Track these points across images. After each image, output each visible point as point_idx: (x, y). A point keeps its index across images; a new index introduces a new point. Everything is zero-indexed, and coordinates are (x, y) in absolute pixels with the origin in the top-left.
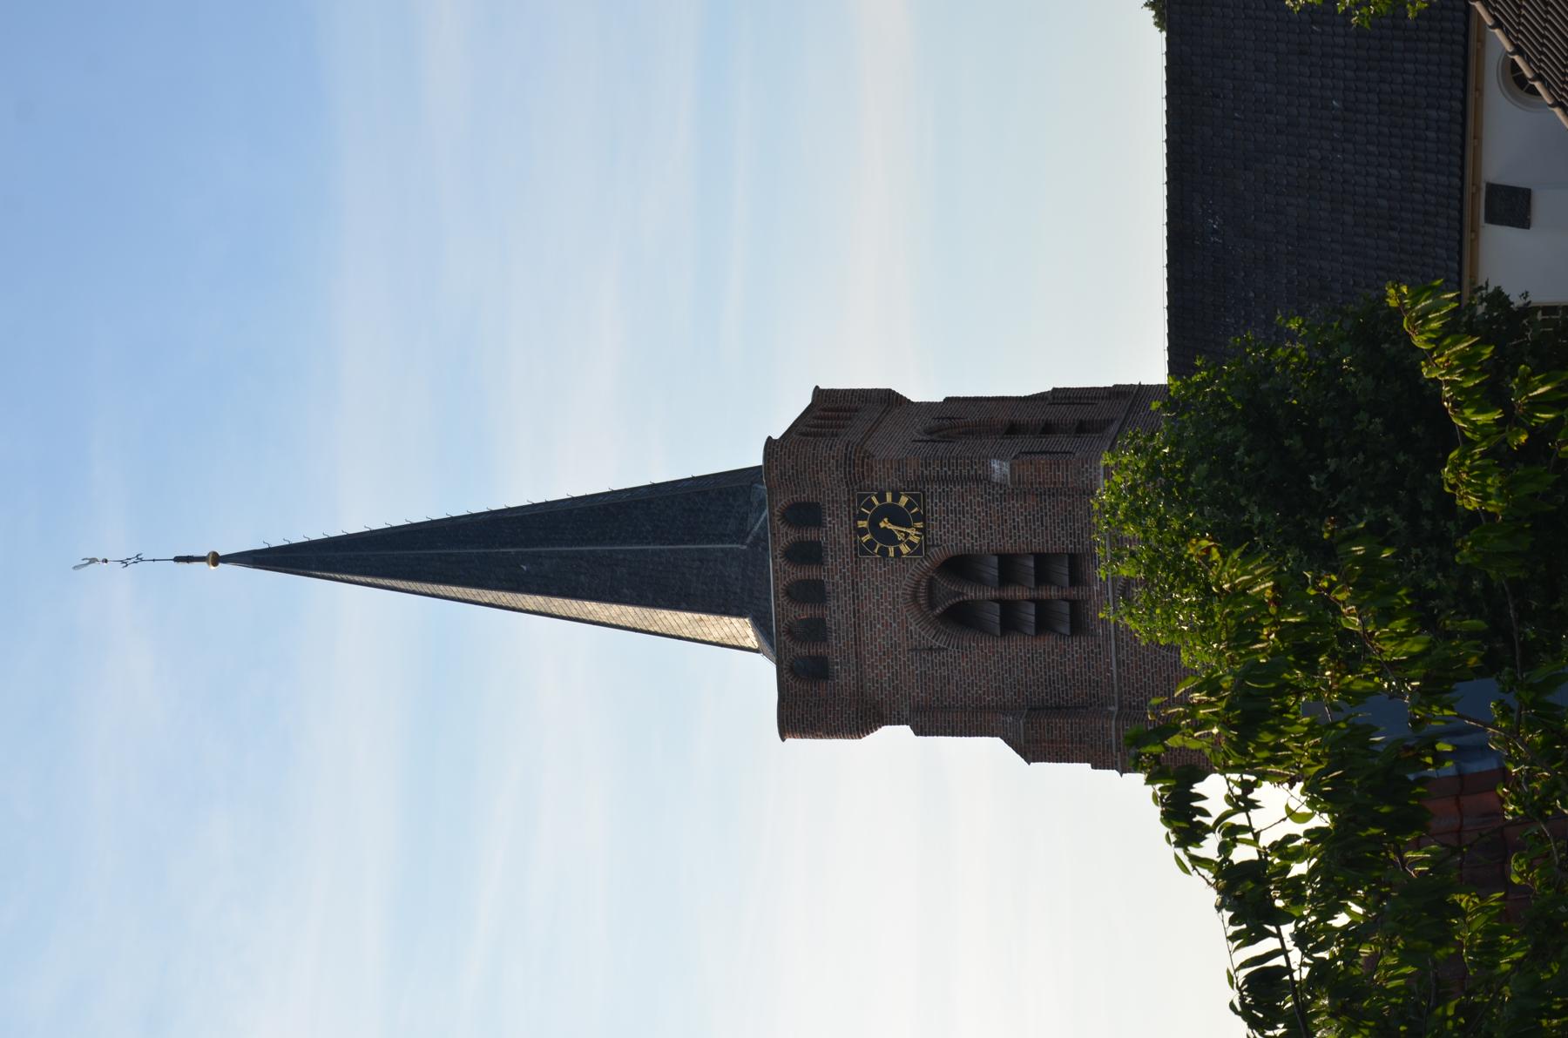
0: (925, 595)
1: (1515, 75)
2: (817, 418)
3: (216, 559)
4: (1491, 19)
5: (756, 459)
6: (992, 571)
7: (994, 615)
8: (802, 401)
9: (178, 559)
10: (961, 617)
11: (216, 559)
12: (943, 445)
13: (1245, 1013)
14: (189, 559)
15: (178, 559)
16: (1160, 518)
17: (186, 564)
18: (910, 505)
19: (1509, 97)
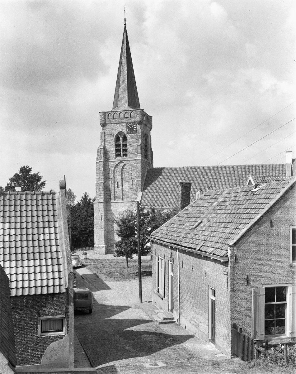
0: (121, 133)
1: (266, 320)
2: (148, 117)
3: (125, 24)
4: (63, 268)
5: (141, 108)
6: (125, 143)
7: (118, 143)
8: (150, 114)
9: (125, 19)
10: (117, 139)
11: (125, 24)
12: (243, 332)
13: (21, 170)
14: (125, 21)
15: (125, 19)
16: (143, 191)
17: (124, 20)
18: (134, 131)
19: (149, 137)
